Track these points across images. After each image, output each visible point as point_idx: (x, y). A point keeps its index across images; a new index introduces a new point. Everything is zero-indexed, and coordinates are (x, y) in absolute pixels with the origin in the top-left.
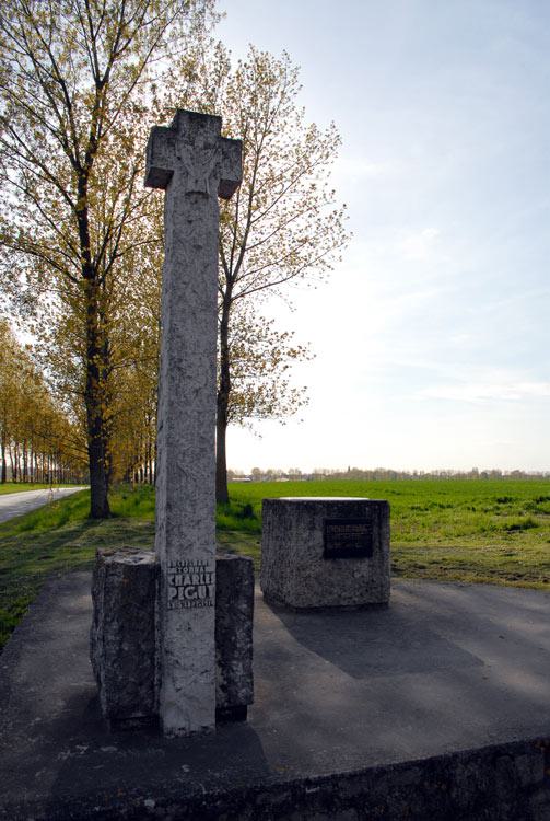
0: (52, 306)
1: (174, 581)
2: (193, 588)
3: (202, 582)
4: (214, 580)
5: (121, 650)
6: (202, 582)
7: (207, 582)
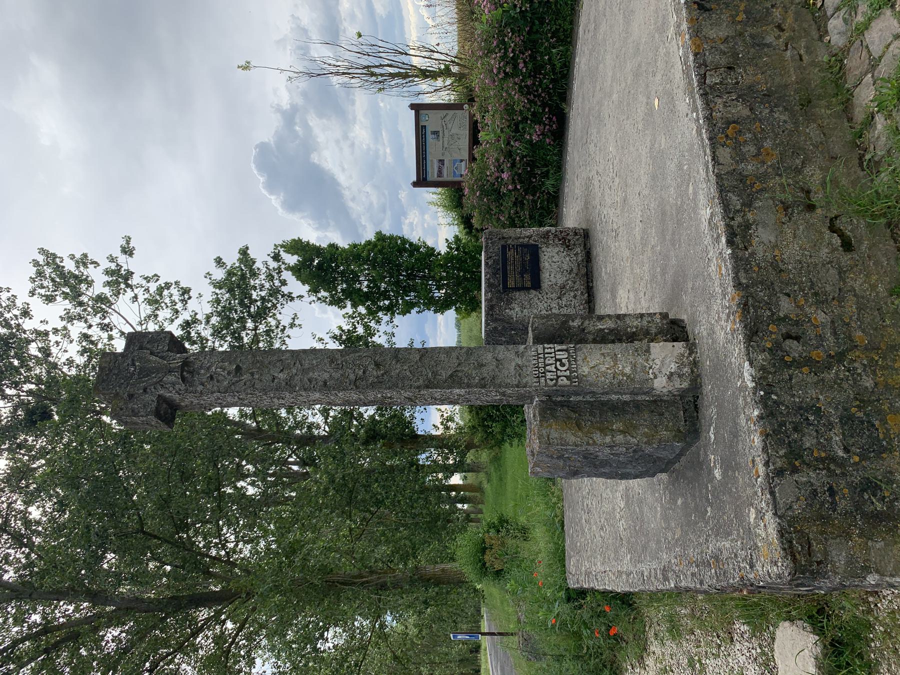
0: (593, 145)
1: (552, 380)
2: (558, 363)
3: (553, 355)
4: (552, 346)
5: (203, 492)
6: (553, 355)
7: (553, 350)
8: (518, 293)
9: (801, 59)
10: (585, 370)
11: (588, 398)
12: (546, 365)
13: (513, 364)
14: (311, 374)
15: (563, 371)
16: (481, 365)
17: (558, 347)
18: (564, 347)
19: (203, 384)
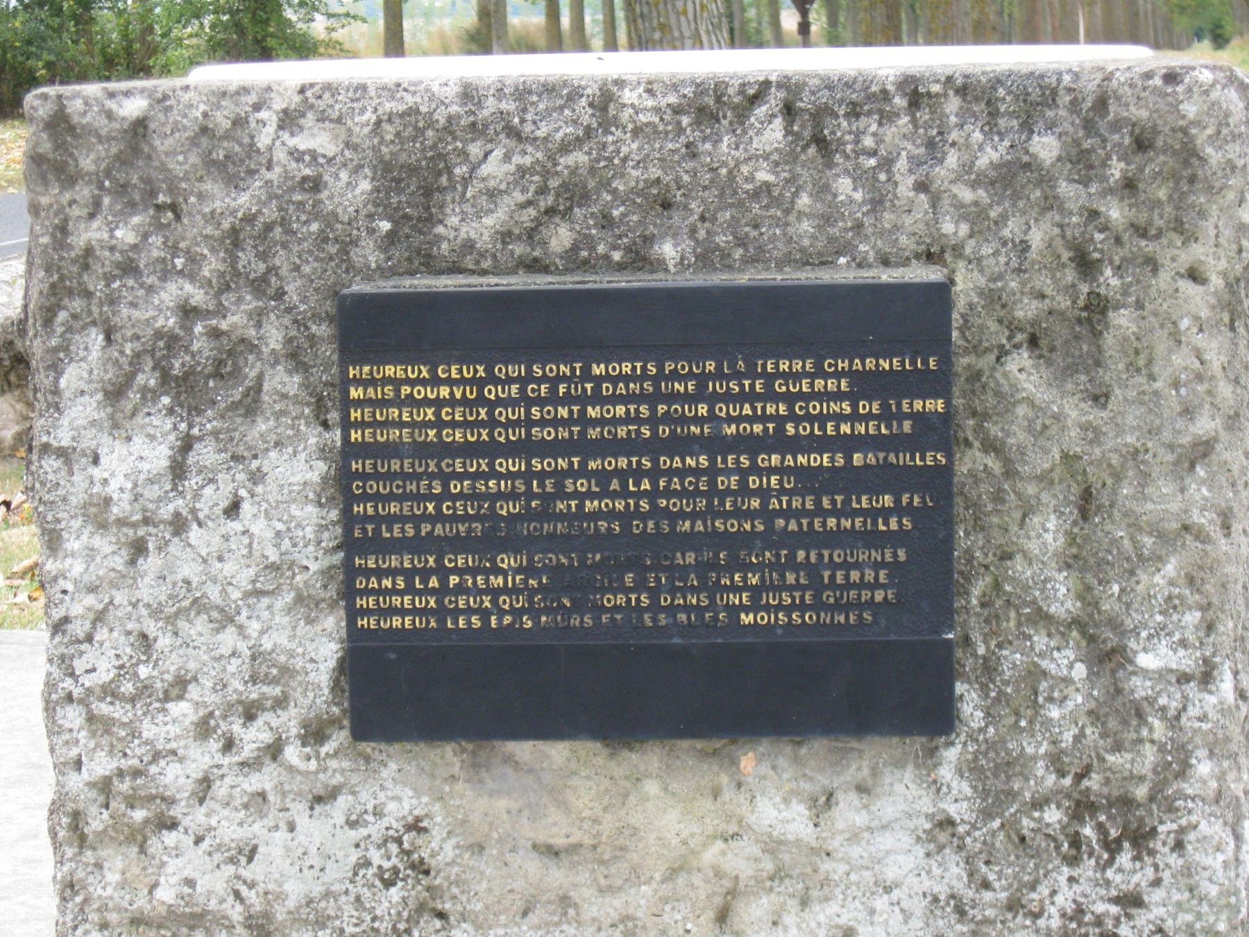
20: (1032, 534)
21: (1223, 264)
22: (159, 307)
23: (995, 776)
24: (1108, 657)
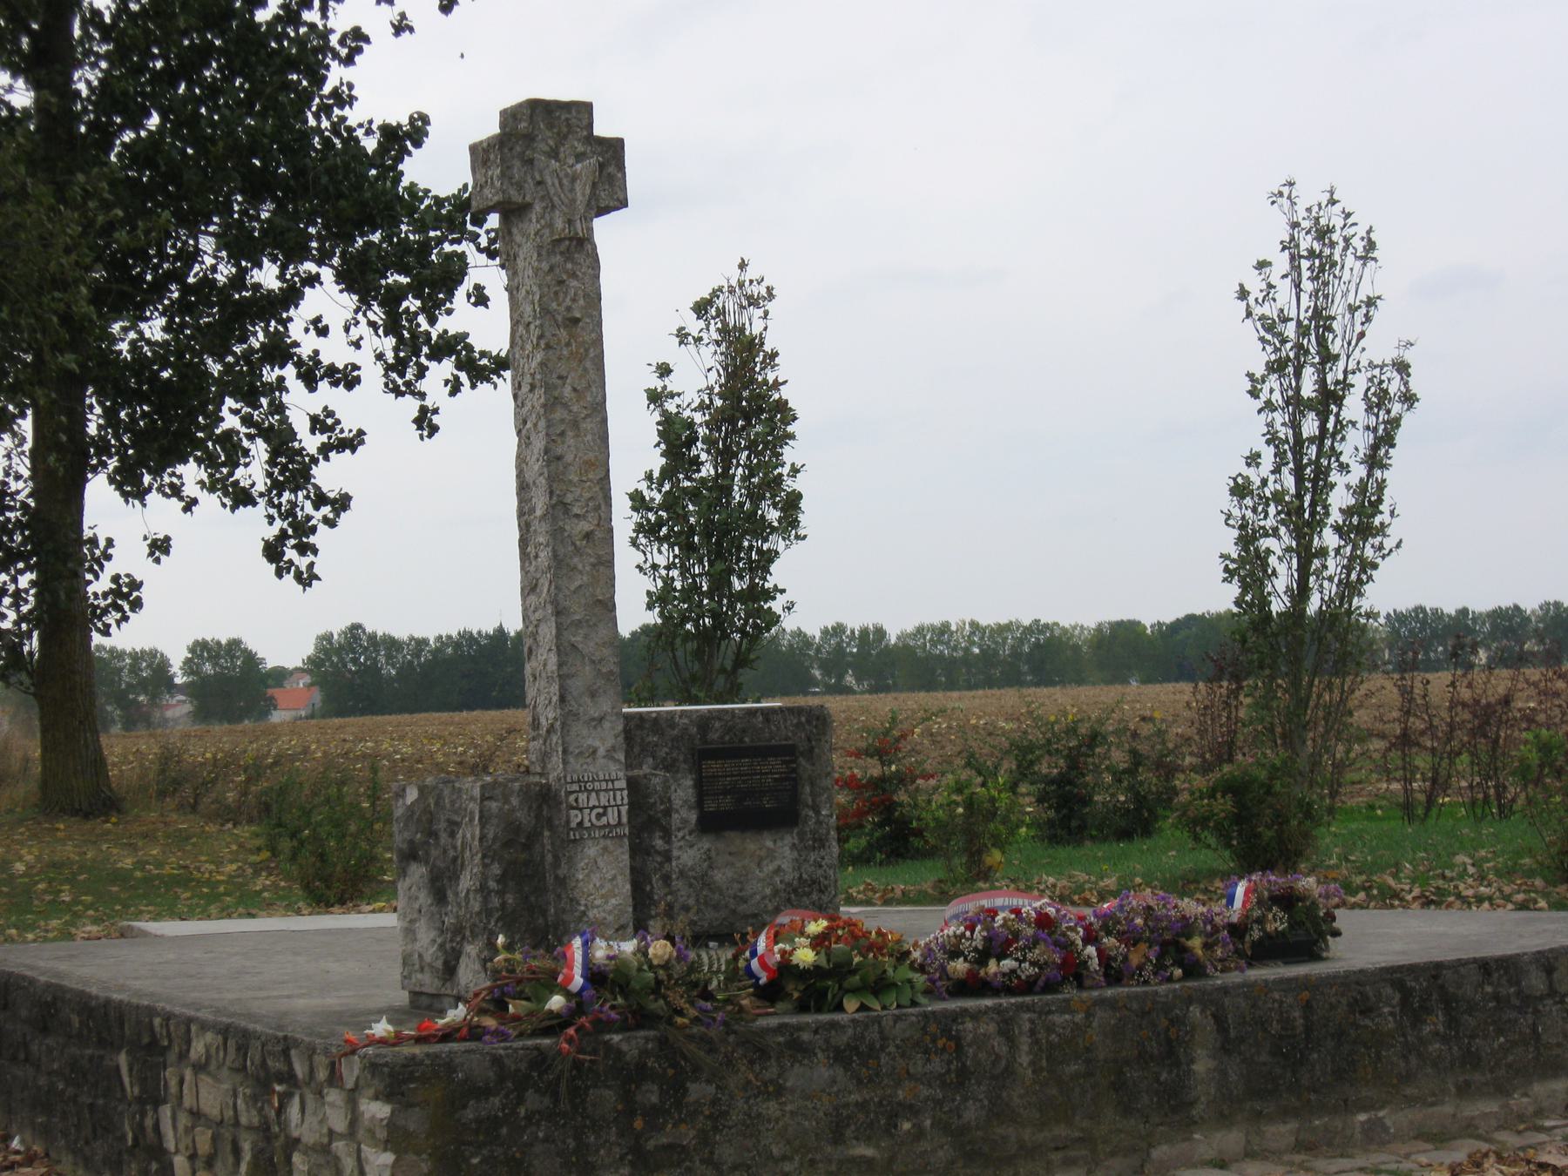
4: (626, 801)
8: (689, 783)
9: (1057, 1149)
10: (592, 851)
11: (549, 858)
12: (597, 792)
13: (597, 743)
14: (570, 434)
15: (589, 818)
16: (593, 695)
17: (624, 809)
18: (625, 820)
19: (551, 269)
20: (757, 1067)
21: (1526, 702)
22: (663, 752)
23: (801, 836)
24: (818, 813)
